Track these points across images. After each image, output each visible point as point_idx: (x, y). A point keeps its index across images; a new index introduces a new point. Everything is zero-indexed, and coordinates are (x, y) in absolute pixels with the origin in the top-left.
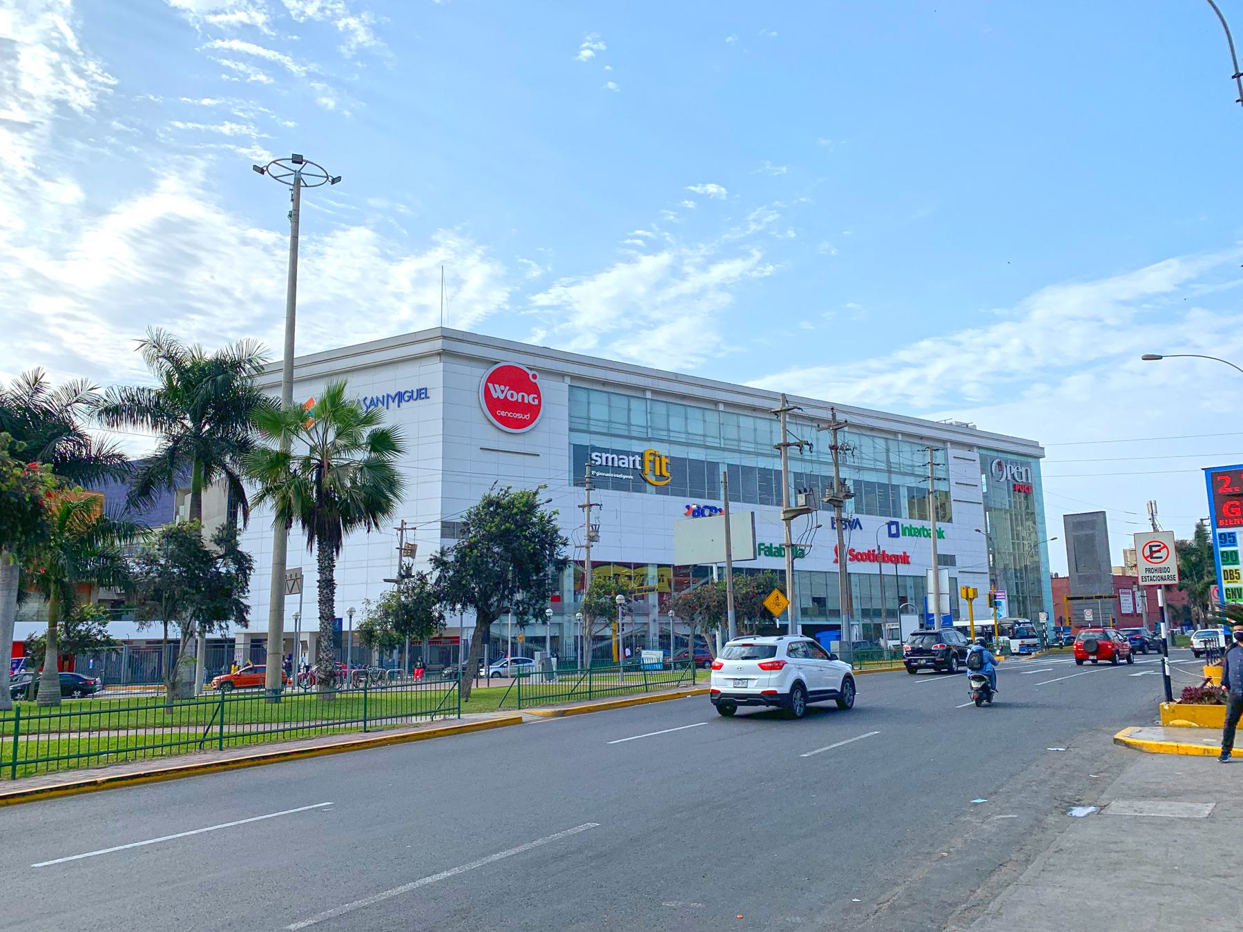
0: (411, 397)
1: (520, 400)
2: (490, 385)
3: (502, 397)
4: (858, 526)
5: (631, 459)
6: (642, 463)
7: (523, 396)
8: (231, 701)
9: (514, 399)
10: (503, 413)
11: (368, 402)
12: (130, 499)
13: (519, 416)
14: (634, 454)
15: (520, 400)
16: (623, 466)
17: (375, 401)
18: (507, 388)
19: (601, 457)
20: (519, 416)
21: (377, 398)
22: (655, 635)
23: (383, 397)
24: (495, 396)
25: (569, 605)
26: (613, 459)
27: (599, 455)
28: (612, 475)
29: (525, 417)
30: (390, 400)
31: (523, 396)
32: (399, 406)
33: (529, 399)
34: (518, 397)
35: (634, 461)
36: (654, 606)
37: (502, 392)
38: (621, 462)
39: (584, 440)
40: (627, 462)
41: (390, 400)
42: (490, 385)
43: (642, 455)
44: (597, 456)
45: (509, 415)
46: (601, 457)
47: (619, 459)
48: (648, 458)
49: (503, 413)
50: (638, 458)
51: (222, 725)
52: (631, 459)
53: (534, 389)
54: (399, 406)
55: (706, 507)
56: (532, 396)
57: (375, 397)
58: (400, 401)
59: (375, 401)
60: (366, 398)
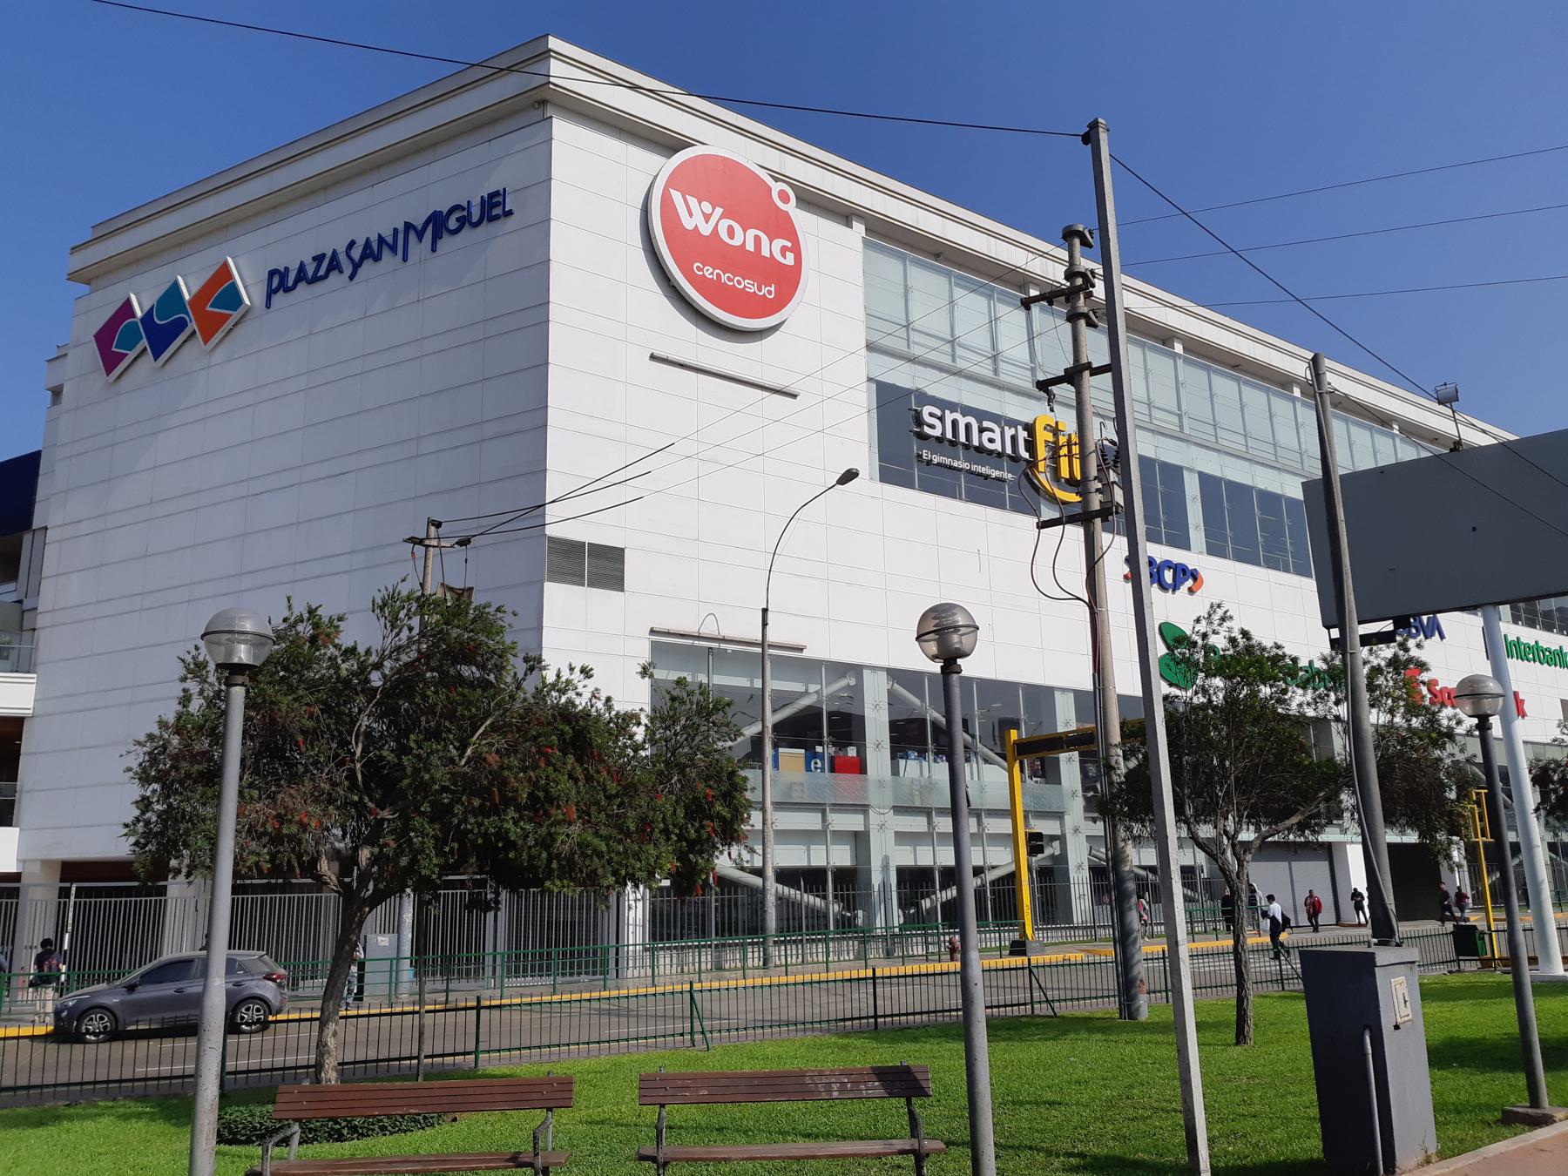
0: (463, 222)
1: (750, 247)
2: (676, 196)
3: (706, 230)
4: (1437, 633)
5: (1009, 432)
6: (1031, 445)
7: (757, 240)
8: (490, 1007)
9: (737, 242)
10: (708, 272)
11: (356, 253)
12: (153, 758)
13: (749, 286)
14: (1013, 423)
15: (750, 247)
16: (990, 446)
17: (375, 246)
18: (719, 211)
19: (941, 419)
20: (749, 286)
21: (381, 240)
22: (1079, 867)
23: (396, 231)
24: (688, 224)
25: (881, 784)
26: (968, 427)
27: (938, 413)
28: (966, 466)
29: (765, 290)
30: (412, 237)
31: (757, 240)
32: (434, 250)
33: (773, 248)
34: (744, 238)
35: (1014, 439)
36: (1074, 794)
37: (707, 218)
38: (986, 435)
39: (903, 376)
40: (995, 439)
41: (412, 237)
42: (676, 196)
43: (1030, 428)
44: (931, 415)
45: (724, 278)
46: (941, 419)
47: (982, 430)
48: (1043, 437)
49: (708, 272)
50: (1023, 435)
51: (894, 927)
52: (1009, 432)
53: (782, 227)
54: (434, 250)
55: (1168, 564)
56: (779, 243)
57: (374, 238)
58: (437, 236)
59: (375, 246)
60: (352, 244)
